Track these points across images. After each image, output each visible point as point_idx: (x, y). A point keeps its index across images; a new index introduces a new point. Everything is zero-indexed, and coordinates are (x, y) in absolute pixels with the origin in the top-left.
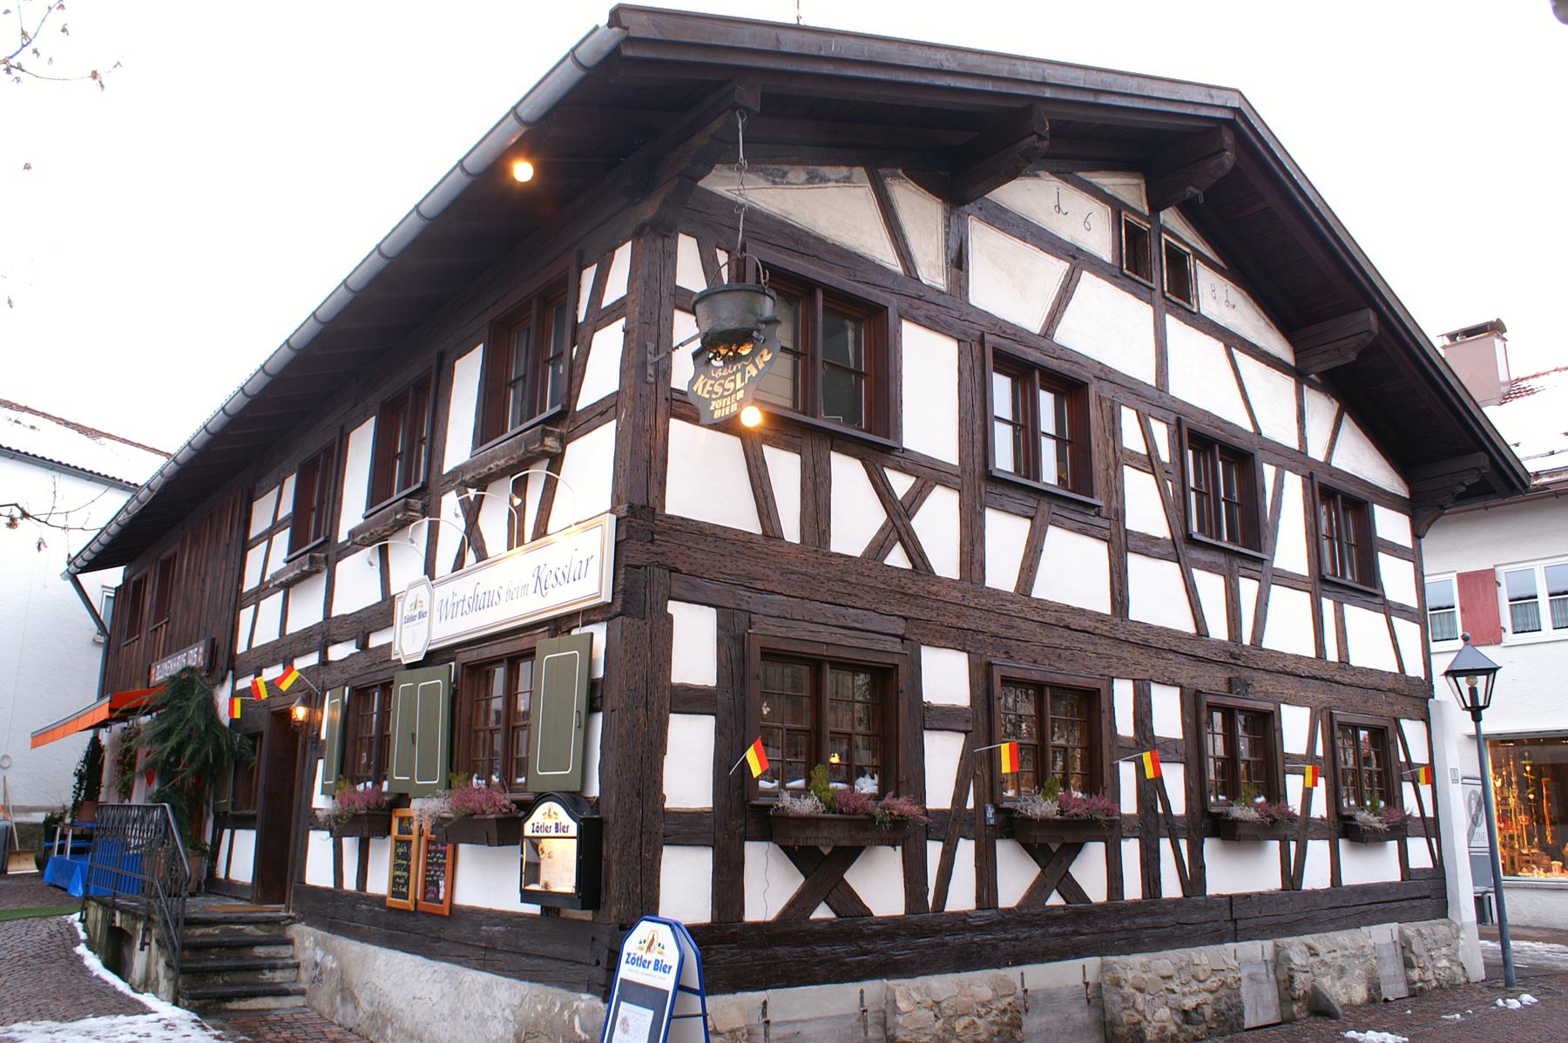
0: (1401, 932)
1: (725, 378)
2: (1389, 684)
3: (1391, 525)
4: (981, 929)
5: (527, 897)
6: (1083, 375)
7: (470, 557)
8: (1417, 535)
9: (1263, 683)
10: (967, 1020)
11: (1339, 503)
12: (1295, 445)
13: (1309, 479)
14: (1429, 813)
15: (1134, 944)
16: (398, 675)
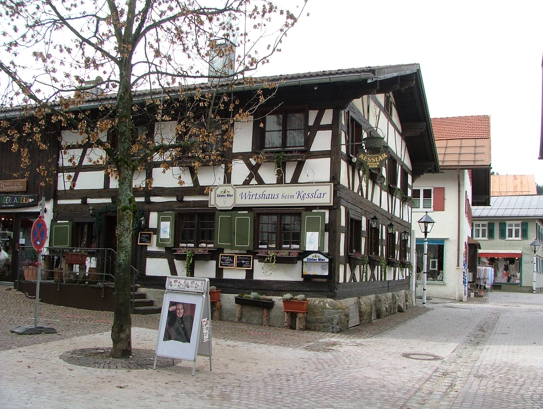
5: (303, 276)
7: (254, 182)
13: (402, 166)
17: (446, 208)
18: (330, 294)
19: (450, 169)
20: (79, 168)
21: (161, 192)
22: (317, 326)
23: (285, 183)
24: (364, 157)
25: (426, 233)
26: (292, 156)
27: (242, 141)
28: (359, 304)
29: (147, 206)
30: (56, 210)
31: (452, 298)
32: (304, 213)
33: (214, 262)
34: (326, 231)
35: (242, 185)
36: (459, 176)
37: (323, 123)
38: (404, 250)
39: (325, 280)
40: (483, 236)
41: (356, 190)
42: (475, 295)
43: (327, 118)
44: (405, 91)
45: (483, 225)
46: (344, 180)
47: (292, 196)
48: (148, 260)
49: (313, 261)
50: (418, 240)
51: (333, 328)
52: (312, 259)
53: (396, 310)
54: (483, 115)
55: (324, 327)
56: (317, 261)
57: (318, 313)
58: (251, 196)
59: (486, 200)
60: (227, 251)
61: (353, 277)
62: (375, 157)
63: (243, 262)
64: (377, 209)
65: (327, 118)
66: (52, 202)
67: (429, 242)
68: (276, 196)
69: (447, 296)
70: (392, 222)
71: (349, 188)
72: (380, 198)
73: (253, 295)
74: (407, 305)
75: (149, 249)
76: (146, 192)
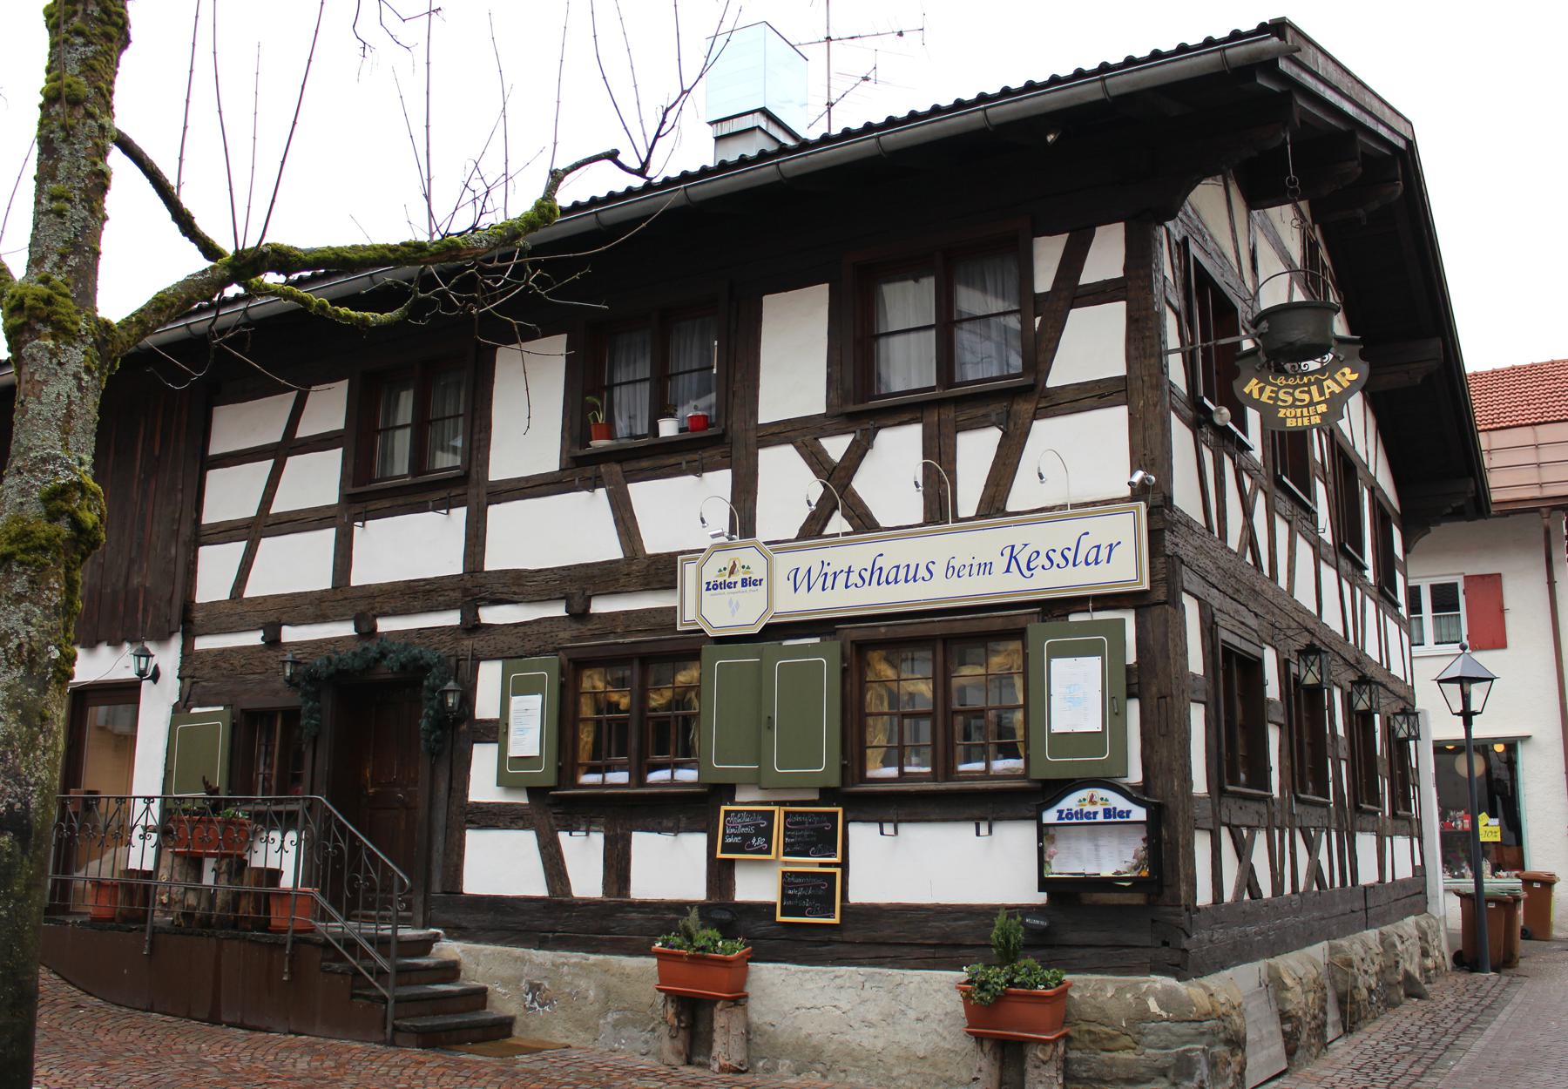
1: (1295, 387)
5: (1044, 884)
7: (838, 523)
13: (1372, 491)
16: (707, 649)
18: (1165, 954)
20: (264, 524)
21: (517, 586)
23: (956, 519)
24: (1261, 391)
25: (1467, 716)
28: (1275, 984)
29: (468, 643)
30: (189, 671)
32: (1034, 628)
34: (1130, 696)
35: (797, 539)
37: (1089, 276)
38: (1404, 780)
41: (1234, 542)
43: (1106, 257)
46: (1186, 497)
47: (986, 568)
48: (473, 838)
49: (1083, 823)
56: (1100, 818)
57: (1112, 1038)
61: (1248, 880)
64: (1311, 626)
65: (1106, 257)
66: (176, 644)
68: (922, 572)
70: (1366, 679)
71: (1209, 528)
72: (1313, 586)
76: (466, 591)
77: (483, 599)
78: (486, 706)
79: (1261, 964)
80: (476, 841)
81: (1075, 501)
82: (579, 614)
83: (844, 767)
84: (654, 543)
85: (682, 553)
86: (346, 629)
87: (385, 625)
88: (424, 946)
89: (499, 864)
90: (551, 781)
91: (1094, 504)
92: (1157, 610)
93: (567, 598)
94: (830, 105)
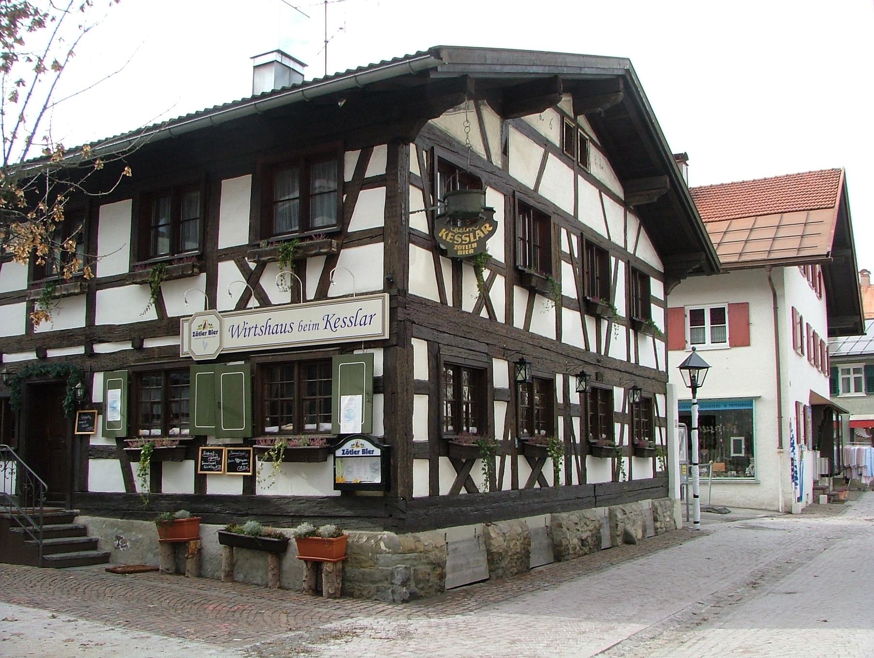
0: (653, 503)
1: (462, 234)
2: (652, 376)
3: (656, 288)
4: (514, 500)
5: (337, 486)
6: (549, 211)
7: (253, 302)
8: (666, 293)
9: (608, 375)
10: (514, 542)
11: (638, 277)
12: (623, 245)
13: (627, 264)
14: (664, 444)
15: (566, 507)
16: (193, 367)
17: (753, 341)
19: (752, 267)
21: (111, 333)
22: (364, 589)
23: (305, 300)
24: (447, 235)
25: (694, 387)
26: (312, 245)
27: (234, 227)
29: (88, 363)
31: (772, 508)
32: (336, 358)
33: (192, 463)
36: (770, 279)
37: (369, 174)
39: (379, 494)
40: (857, 389)
42: (829, 499)
43: (377, 165)
44: (608, 114)
45: (856, 371)
49: (352, 455)
50: (682, 403)
51: (393, 592)
52: (352, 452)
53: (619, 540)
54: (831, 168)
55: (378, 590)
57: (365, 561)
58: (248, 331)
59: (856, 324)
60: (212, 442)
62: (469, 232)
63: (238, 461)
65: (377, 165)
67: (700, 406)
68: (288, 328)
69: (762, 504)
73: (250, 525)
74: (656, 529)
75: (93, 442)
76: (87, 336)
77: (94, 340)
78: (97, 396)
79: (479, 527)
80: (94, 465)
81: (358, 292)
82: (138, 348)
83: (253, 427)
84: (171, 312)
85: (184, 317)
86: (32, 356)
87: (52, 353)
88: (70, 518)
89: (104, 476)
90: (124, 435)
91: (366, 294)
92: (392, 349)
93: (132, 339)
94: (326, 42)
